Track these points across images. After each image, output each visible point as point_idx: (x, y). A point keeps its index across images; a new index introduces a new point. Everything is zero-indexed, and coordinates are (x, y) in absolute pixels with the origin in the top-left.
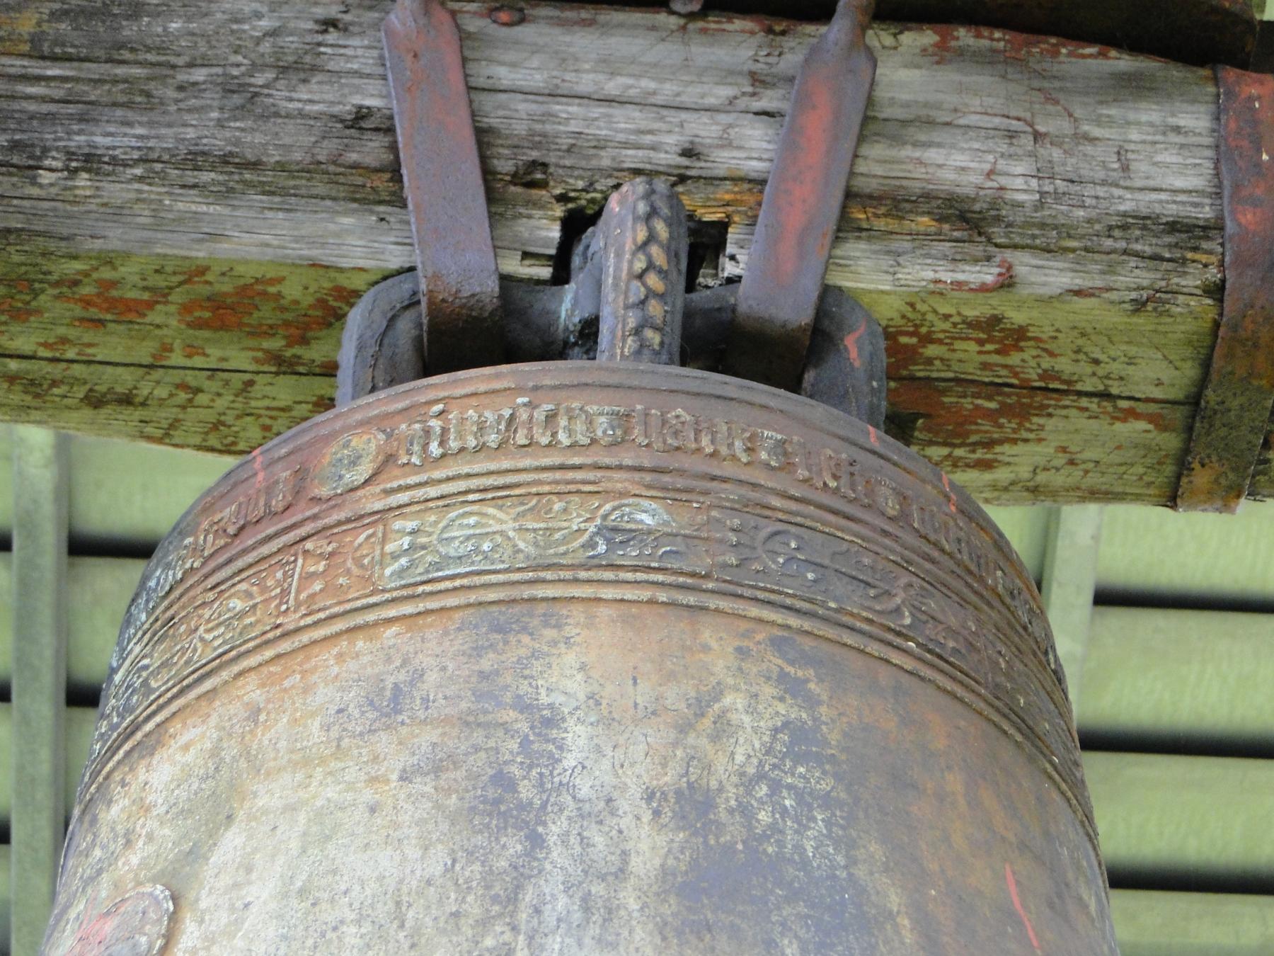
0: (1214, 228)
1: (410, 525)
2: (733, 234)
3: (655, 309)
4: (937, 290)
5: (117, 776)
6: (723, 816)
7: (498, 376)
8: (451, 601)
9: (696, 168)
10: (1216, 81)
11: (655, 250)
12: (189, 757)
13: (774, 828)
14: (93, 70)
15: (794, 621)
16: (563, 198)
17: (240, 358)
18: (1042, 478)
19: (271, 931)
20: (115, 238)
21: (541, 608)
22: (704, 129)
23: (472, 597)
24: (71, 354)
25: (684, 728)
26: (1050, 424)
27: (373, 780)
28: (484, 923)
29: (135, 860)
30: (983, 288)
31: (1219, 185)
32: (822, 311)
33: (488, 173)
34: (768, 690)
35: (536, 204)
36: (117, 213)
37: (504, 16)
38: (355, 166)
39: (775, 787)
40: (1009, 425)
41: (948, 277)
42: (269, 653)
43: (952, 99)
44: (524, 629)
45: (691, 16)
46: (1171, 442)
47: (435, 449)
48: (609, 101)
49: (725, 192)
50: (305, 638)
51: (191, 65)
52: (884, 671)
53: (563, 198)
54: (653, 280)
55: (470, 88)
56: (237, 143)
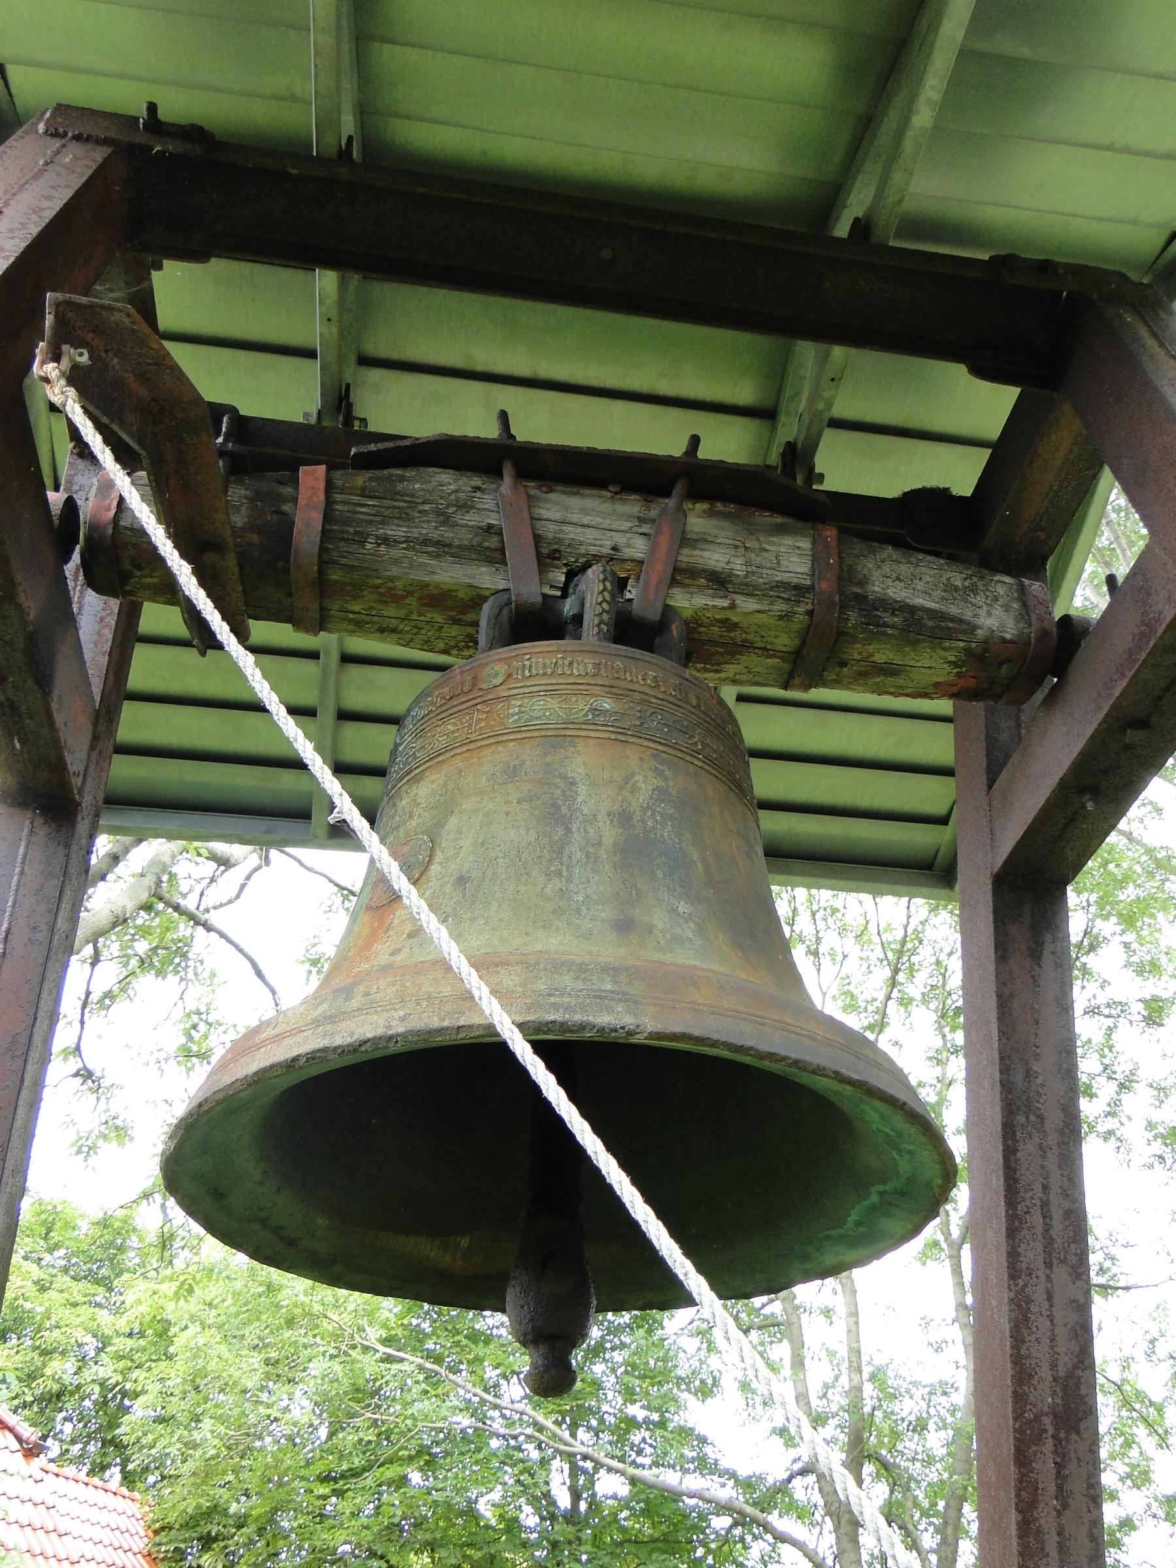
0: (811, 588)
1: (519, 703)
2: (631, 582)
3: (605, 617)
4: (706, 608)
5: (404, 789)
6: (636, 823)
7: (550, 645)
8: (535, 734)
9: (618, 555)
10: (814, 528)
11: (606, 594)
12: (434, 786)
13: (654, 828)
14: (387, 503)
15: (660, 748)
16: (566, 565)
17: (439, 618)
18: (737, 677)
19: (471, 858)
20: (394, 571)
21: (568, 739)
22: (620, 539)
23: (543, 733)
24: (374, 613)
25: (621, 788)
26: (743, 658)
27: (507, 802)
28: (551, 861)
29: (414, 824)
30: (724, 608)
31: (814, 571)
32: (663, 614)
33: (539, 555)
34: (651, 774)
35: (557, 567)
36: (395, 561)
37: (544, 489)
38: (488, 548)
39: (654, 812)
40: (728, 658)
41: (711, 603)
42: (465, 749)
43: (714, 532)
44: (562, 747)
45: (616, 493)
46: (787, 667)
47: (527, 673)
48: (583, 526)
49: (628, 566)
50: (479, 744)
51: (423, 503)
52: (691, 767)
53: (566, 565)
54: (605, 606)
55: (532, 518)
56: (442, 536)
